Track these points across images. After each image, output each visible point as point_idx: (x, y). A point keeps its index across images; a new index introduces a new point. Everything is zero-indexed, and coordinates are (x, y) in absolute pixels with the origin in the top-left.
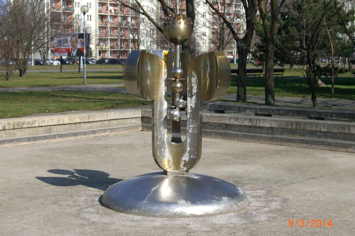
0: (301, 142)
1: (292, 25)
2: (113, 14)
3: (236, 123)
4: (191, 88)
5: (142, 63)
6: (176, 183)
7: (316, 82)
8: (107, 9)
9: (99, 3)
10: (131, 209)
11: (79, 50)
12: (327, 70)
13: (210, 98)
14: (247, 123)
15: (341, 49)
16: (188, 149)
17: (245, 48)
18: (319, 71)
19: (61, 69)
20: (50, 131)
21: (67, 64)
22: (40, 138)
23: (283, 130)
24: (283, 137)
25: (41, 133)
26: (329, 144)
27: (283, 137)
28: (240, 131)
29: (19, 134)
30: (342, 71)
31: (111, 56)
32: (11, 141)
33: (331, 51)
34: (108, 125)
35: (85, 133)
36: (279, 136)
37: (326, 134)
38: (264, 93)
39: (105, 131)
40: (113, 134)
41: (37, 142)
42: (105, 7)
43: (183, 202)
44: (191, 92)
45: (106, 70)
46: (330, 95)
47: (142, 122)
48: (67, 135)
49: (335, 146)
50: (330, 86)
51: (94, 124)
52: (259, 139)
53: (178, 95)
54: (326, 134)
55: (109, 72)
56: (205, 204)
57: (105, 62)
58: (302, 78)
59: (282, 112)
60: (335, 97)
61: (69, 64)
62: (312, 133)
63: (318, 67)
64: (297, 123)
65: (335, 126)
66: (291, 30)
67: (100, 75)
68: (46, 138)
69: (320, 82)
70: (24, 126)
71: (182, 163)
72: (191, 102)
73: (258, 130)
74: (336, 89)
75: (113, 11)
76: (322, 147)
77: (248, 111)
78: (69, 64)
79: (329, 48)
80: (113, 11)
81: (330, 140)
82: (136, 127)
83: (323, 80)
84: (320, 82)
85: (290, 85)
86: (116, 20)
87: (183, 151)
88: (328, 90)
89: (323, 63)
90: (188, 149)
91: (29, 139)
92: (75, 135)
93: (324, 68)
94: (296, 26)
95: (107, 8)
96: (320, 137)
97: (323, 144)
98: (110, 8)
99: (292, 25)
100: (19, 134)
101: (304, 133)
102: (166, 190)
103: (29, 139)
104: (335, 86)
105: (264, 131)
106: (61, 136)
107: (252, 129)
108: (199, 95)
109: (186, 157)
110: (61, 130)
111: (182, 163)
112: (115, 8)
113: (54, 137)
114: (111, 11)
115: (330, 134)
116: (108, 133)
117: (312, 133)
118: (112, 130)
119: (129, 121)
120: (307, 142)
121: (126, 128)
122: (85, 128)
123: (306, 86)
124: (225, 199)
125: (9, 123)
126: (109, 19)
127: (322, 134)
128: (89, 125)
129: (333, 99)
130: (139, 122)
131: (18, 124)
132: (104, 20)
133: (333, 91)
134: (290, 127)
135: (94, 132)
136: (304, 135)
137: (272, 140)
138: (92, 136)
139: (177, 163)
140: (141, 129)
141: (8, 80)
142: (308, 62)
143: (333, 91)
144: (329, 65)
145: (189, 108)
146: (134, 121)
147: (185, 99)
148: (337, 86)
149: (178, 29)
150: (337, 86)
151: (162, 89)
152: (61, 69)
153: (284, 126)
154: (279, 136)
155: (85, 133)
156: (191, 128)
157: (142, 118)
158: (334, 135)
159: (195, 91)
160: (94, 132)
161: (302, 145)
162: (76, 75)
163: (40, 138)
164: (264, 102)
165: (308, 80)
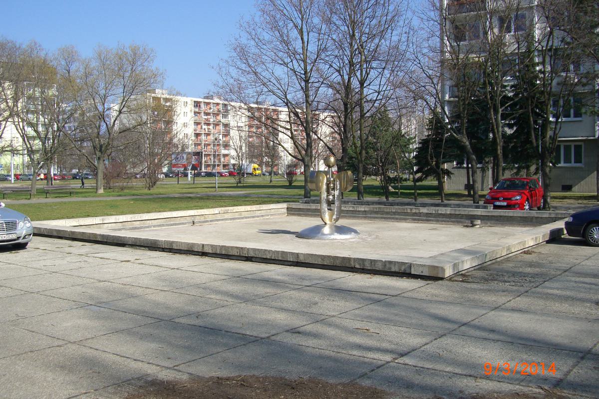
0: (382, 218)
1: (371, 148)
2: (207, 132)
3: (345, 209)
4: (337, 186)
5: (317, 176)
6: (331, 227)
7: (388, 187)
8: (201, 128)
9: (194, 122)
10: (314, 237)
11: (193, 165)
12: (395, 180)
13: (346, 190)
14: (351, 209)
15: (404, 165)
16: (336, 213)
17: (342, 165)
18: (389, 180)
19: (194, 181)
20: (241, 215)
21: (170, 177)
22: (236, 219)
23: (372, 212)
24: (372, 216)
25: (237, 215)
26: (397, 219)
27: (372, 216)
28: (347, 214)
29: (226, 216)
30: (406, 180)
31: (205, 169)
32: (222, 220)
33: (398, 167)
34: (270, 213)
35: (258, 217)
36: (369, 216)
37: (395, 213)
38: (357, 195)
39: (268, 215)
40: (272, 217)
41: (235, 221)
42: (199, 126)
43: (336, 234)
44: (337, 188)
45: (224, 182)
46: (397, 196)
47: (287, 211)
48: (249, 217)
49: (400, 219)
50: (397, 191)
51: (262, 211)
52: (358, 218)
53: (330, 189)
54: (395, 213)
55: (224, 184)
56: (345, 234)
57: (201, 175)
58: (376, 186)
59: (368, 203)
60: (401, 197)
61: (172, 177)
62: (387, 213)
63: (389, 177)
64: (379, 208)
65: (399, 208)
66: (370, 152)
67: (223, 185)
68: (239, 218)
69: (390, 188)
70: (229, 212)
71: (333, 220)
72: (337, 193)
73: (357, 213)
74: (401, 193)
75: (207, 130)
76: (393, 220)
77: (349, 204)
78: (172, 177)
79: (396, 164)
80: (207, 130)
81: (397, 216)
82: (284, 214)
83: (392, 187)
84: (390, 188)
85: (551, 107)
86: (209, 137)
87: (333, 214)
88: (396, 193)
89: (392, 174)
90: (336, 213)
91: (231, 219)
92: (253, 217)
93: (393, 178)
94: (373, 148)
95: (202, 126)
96: (391, 215)
97: (393, 218)
98: (204, 127)
99: (371, 148)
100: (226, 216)
101: (383, 213)
102: (326, 230)
103: (231, 219)
104: (401, 191)
105: (361, 213)
106: (246, 218)
107: (354, 212)
108: (340, 189)
109: (334, 217)
110: (246, 214)
111: (333, 220)
112: (208, 127)
113: (243, 218)
114: (205, 129)
115: (397, 213)
116: (269, 217)
117: (387, 213)
118: (271, 215)
119: (280, 210)
120: (385, 218)
121: (279, 214)
122: (258, 213)
123: (382, 191)
124: (353, 233)
125: (222, 210)
126: (203, 137)
127: (393, 213)
128: (260, 212)
129: (399, 199)
130: (285, 211)
131: (226, 210)
132: (199, 138)
133: (399, 193)
134: (375, 210)
135: (262, 216)
136: (383, 214)
137: (365, 218)
138: (261, 218)
139: (331, 220)
140: (286, 215)
141: (150, 190)
142: (383, 174)
143: (399, 193)
144: (396, 176)
145: (336, 195)
146: (283, 210)
147: (334, 191)
148: (403, 191)
149: (330, 161)
150: (403, 191)
151: (325, 187)
152: (194, 181)
153: (372, 210)
154: (369, 216)
155: (258, 217)
156: (337, 203)
157: (287, 208)
158: (399, 214)
159: (338, 188)
160: (262, 216)
161: (382, 220)
162: (191, 186)
163: (236, 219)
164: (357, 198)
165: (382, 187)
